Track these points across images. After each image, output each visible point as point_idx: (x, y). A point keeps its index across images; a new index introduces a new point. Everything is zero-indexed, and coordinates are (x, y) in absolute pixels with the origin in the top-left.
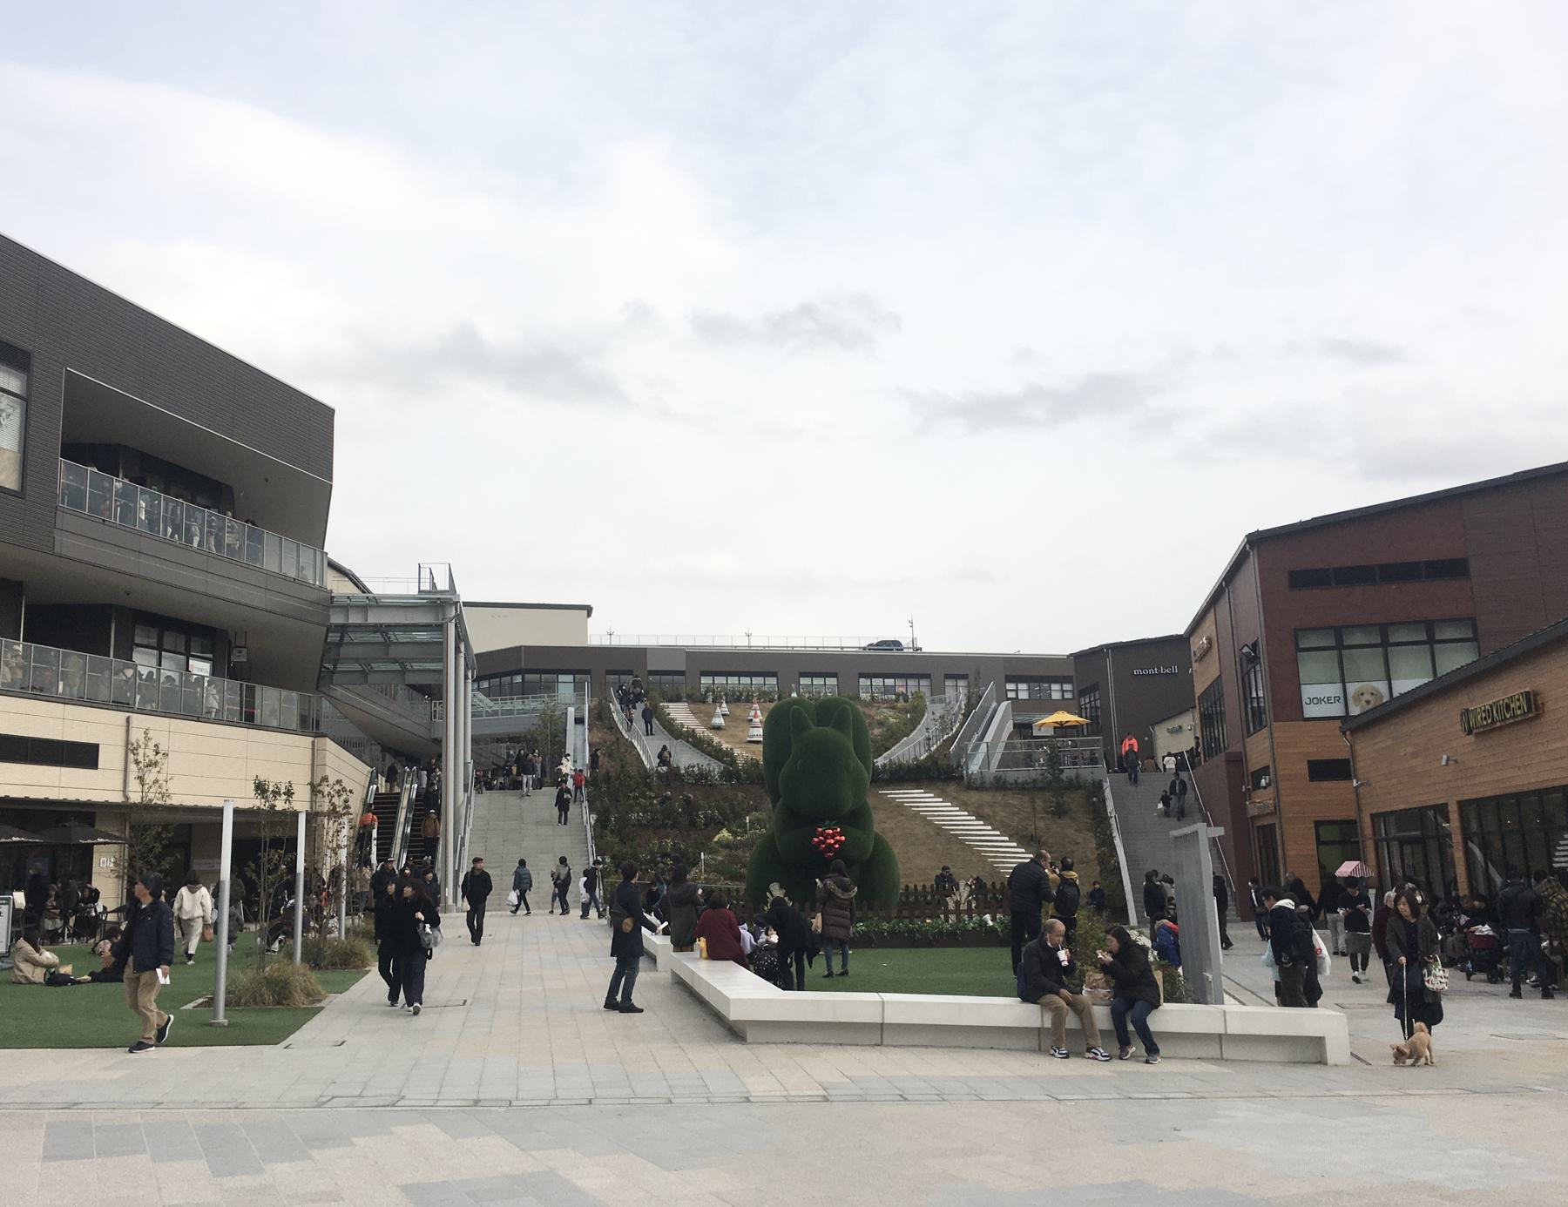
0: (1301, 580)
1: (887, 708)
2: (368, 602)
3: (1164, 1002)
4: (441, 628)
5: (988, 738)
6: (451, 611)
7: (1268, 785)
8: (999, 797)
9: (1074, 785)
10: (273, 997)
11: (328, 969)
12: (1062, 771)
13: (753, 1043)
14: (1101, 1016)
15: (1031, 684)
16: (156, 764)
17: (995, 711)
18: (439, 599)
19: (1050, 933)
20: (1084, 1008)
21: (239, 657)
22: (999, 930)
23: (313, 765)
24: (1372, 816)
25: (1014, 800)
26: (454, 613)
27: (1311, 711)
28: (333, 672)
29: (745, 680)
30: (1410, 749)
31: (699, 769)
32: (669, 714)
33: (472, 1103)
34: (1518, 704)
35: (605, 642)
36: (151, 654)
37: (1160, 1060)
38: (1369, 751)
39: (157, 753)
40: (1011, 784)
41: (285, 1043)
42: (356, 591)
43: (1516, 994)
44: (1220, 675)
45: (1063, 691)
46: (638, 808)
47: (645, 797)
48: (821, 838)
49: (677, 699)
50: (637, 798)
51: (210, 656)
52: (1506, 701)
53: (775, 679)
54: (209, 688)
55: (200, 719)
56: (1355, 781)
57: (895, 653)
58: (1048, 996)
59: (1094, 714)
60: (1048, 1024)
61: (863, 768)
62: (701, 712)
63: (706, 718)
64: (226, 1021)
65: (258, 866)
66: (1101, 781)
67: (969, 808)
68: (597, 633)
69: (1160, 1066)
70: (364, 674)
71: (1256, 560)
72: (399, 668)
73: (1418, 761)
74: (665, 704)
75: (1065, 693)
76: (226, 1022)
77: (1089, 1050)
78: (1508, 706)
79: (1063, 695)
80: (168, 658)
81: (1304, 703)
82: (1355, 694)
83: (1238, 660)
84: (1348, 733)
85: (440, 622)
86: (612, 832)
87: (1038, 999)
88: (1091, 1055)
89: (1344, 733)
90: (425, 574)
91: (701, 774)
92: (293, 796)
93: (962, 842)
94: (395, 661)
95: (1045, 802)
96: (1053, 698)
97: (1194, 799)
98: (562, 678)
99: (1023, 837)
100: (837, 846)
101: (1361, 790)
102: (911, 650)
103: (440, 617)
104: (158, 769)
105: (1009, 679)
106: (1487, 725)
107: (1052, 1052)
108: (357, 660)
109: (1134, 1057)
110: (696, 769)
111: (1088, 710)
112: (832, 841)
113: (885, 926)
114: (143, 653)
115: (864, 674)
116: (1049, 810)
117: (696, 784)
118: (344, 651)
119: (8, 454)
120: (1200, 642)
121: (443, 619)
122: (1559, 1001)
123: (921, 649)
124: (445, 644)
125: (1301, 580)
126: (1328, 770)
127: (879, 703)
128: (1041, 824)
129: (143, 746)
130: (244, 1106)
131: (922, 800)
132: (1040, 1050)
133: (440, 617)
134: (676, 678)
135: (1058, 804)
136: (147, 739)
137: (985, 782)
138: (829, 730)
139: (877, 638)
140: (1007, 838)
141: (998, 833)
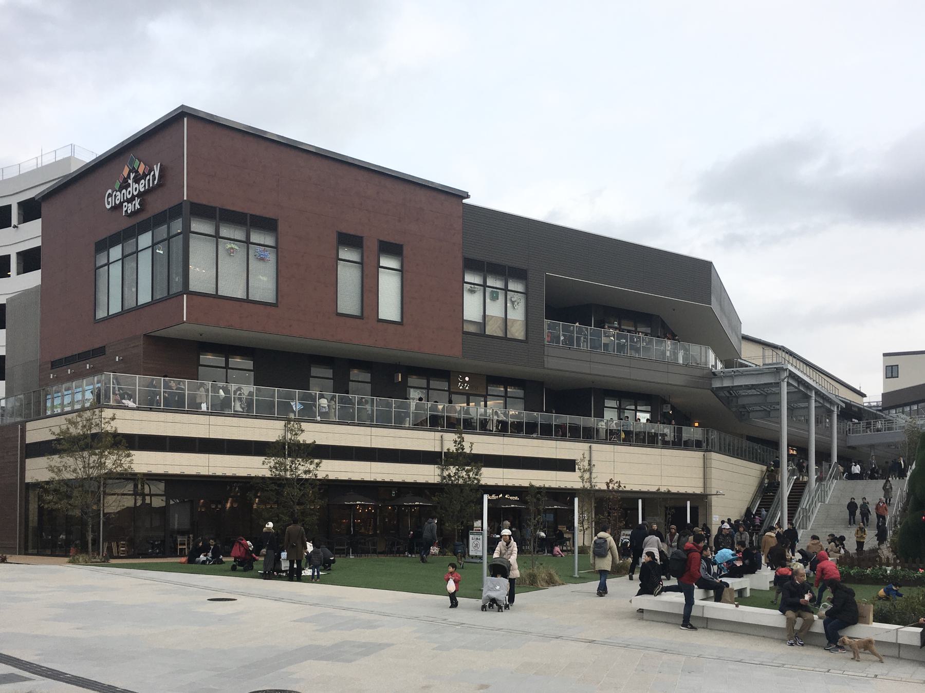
3: (874, 621)
4: (778, 385)
14: (819, 626)
19: (796, 575)
36: (615, 411)
119: (519, 323)
121: (779, 380)
130: (701, 656)
132: (783, 641)
133: (778, 378)
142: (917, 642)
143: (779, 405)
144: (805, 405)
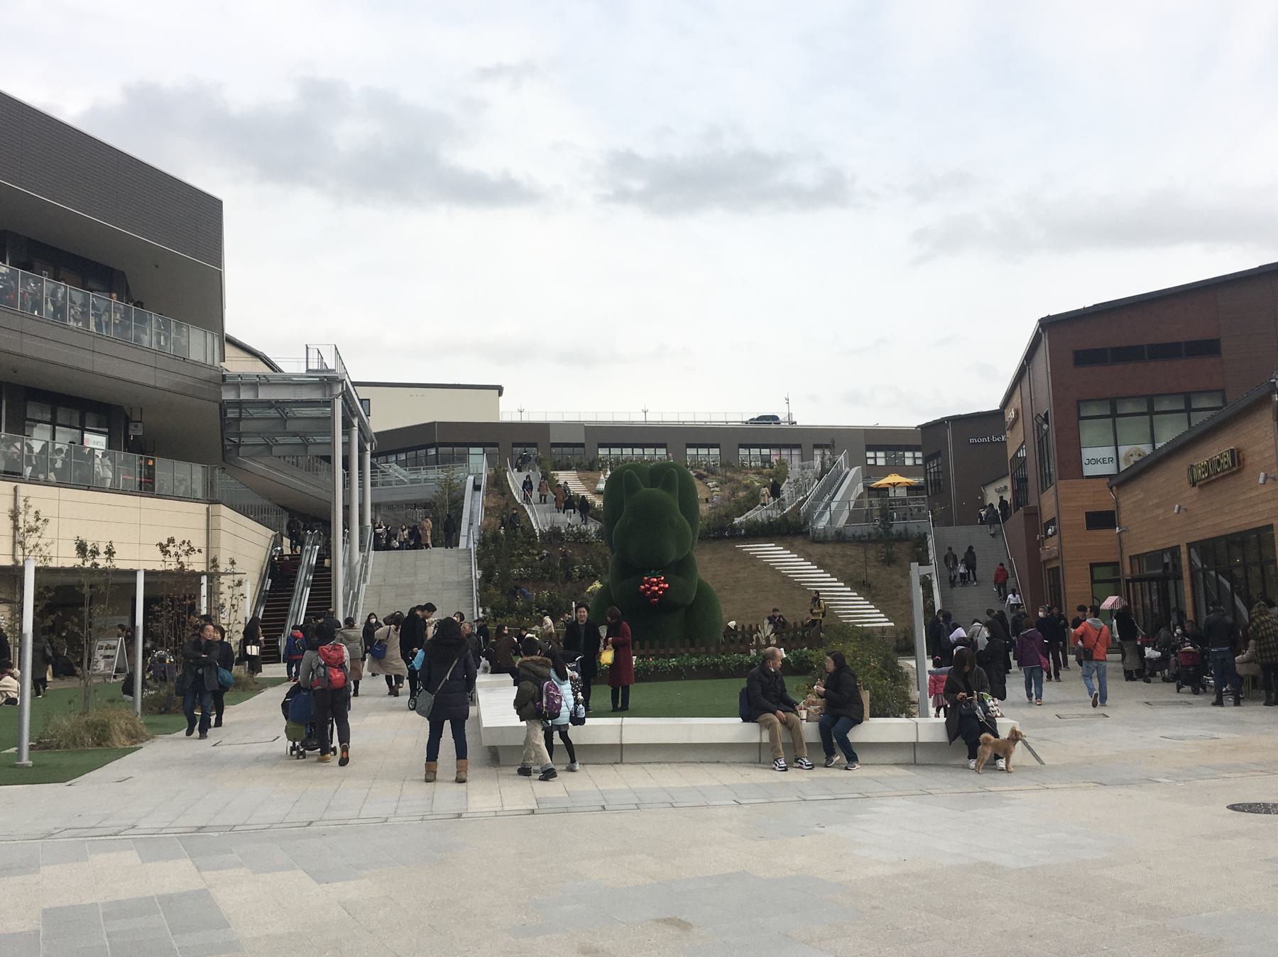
0: (1085, 358)
1: (754, 474)
2: (258, 380)
4: (329, 403)
5: (838, 497)
6: (338, 389)
7: (1054, 533)
8: (839, 548)
9: (903, 537)
10: (93, 739)
11: (177, 713)
12: (891, 525)
13: (627, 763)
14: (809, 731)
15: (888, 452)
16: (36, 529)
17: (848, 473)
18: (325, 377)
20: (794, 724)
21: (136, 431)
22: (791, 661)
23: (208, 530)
24: (1131, 557)
25: (851, 551)
26: (340, 390)
27: (1089, 470)
28: (239, 446)
29: (638, 451)
30: (1156, 501)
31: (578, 529)
32: (557, 481)
33: (456, 816)
34: (1225, 460)
35: (516, 418)
37: (859, 766)
38: (1130, 502)
39: (37, 520)
40: (850, 538)
41: (69, 783)
42: (267, 370)
43: (1219, 703)
44: (1024, 441)
45: (915, 458)
46: (520, 564)
47: (529, 554)
48: (646, 585)
49: (567, 468)
50: (522, 555)
51: (106, 430)
52: (1218, 457)
53: (665, 449)
54: (103, 460)
55: (91, 488)
56: (1117, 528)
57: (773, 426)
58: (771, 714)
59: (937, 478)
60: (766, 739)
61: (688, 524)
62: (588, 479)
63: (592, 484)
64: (31, 762)
65: (82, 620)
66: (926, 533)
67: (812, 559)
68: (509, 411)
69: (858, 771)
70: (269, 447)
71: (1047, 340)
72: (300, 441)
73: (1160, 511)
74: (555, 472)
75: (917, 460)
76: (30, 763)
77: (796, 761)
78: (1219, 461)
79: (915, 462)
80: (63, 432)
81: (1083, 464)
82: (1126, 455)
83: (1035, 428)
84: (1114, 488)
85: (327, 398)
86: (495, 585)
87: (756, 719)
88: (798, 765)
89: (1111, 488)
90: (313, 355)
91: (579, 533)
92: (114, 555)
93: (804, 588)
94: (295, 434)
95: (877, 552)
96: (906, 464)
97: (1003, 547)
98: (472, 450)
99: (857, 582)
100: (661, 592)
101: (1123, 535)
102: (787, 424)
103: (327, 393)
104: (39, 534)
105: (869, 448)
106: (1206, 478)
107: (774, 766)
108: (258, 434)
109: (838, 766)
110: (575, 529)
111: (932, 475)
112: (657, 588)
113: (695, 660)
114: (42, 428)
115: (743, 444)
116: (880, 559)
117: (575, 542)
118: (243, 426)
120: (1010, 415)
121: (331, 396)
122: (1246, 708)
123: (795, 423)
124: (332, 418)
125: (1085, 358)
126: (1101, 520)
127: (748, 469)
128: (871, 571)
129: (23, 513)
131: (774, 553)
133: (327, 393)
134: (576, 449)
135: (888, 553)
136: (27, 507)
137: (827, 537)
138: (657, 491)
139: (758, 413)
140: (842, 584)
141: (836, 579)
142: (941, 736)
143: (330, 436)
144: (327, 439)
